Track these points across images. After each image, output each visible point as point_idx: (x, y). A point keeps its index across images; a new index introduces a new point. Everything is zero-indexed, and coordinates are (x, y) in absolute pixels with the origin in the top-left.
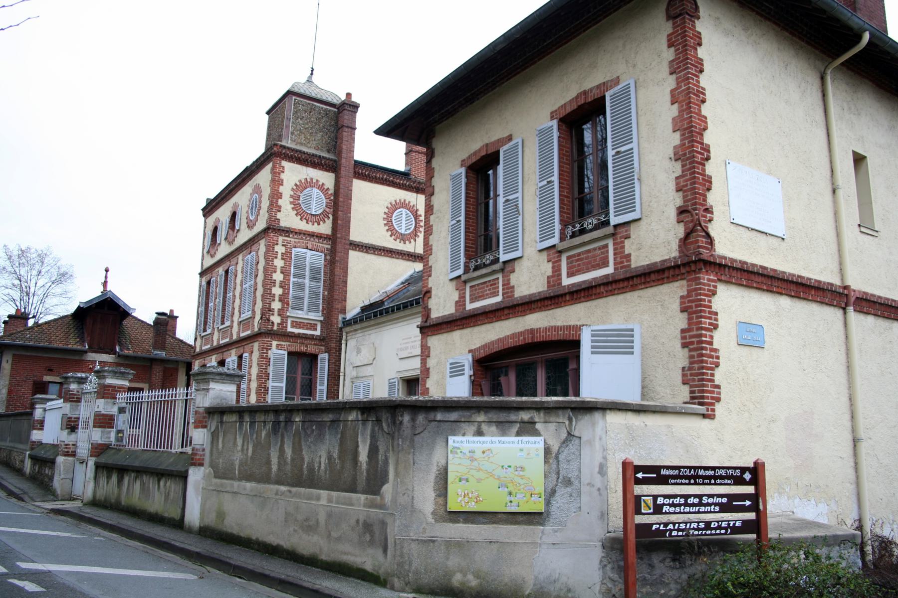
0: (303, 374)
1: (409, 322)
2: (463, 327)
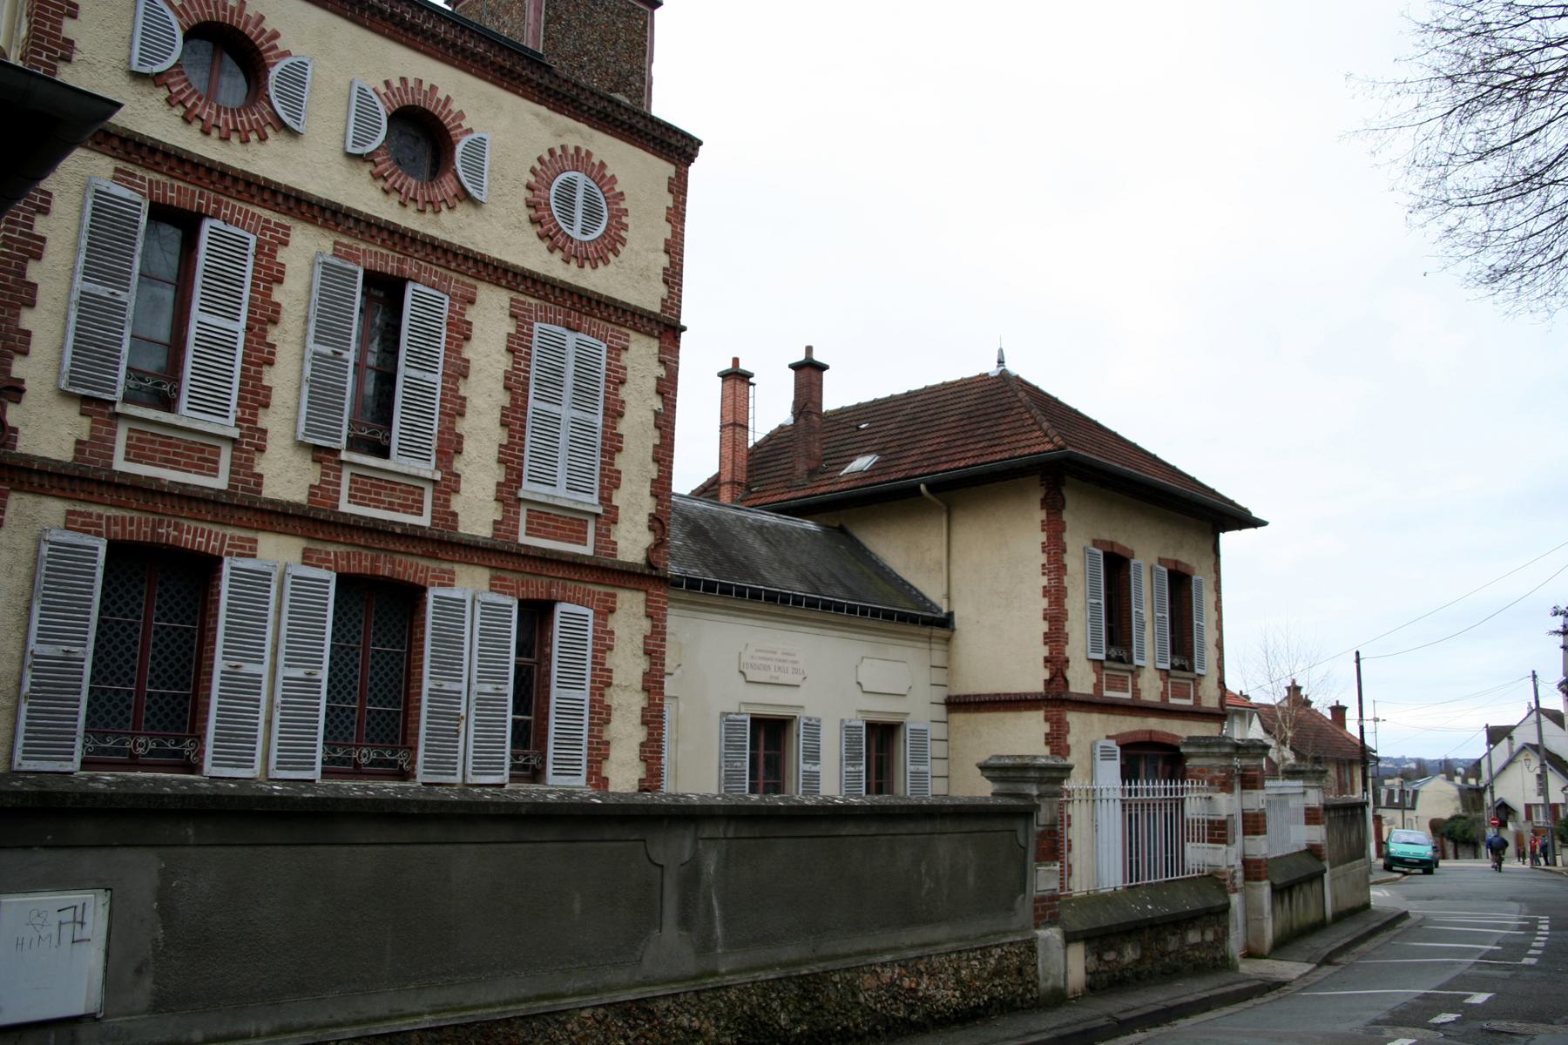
0: (1476, 856)
1: (767, 624)
2: (1101, 712)
